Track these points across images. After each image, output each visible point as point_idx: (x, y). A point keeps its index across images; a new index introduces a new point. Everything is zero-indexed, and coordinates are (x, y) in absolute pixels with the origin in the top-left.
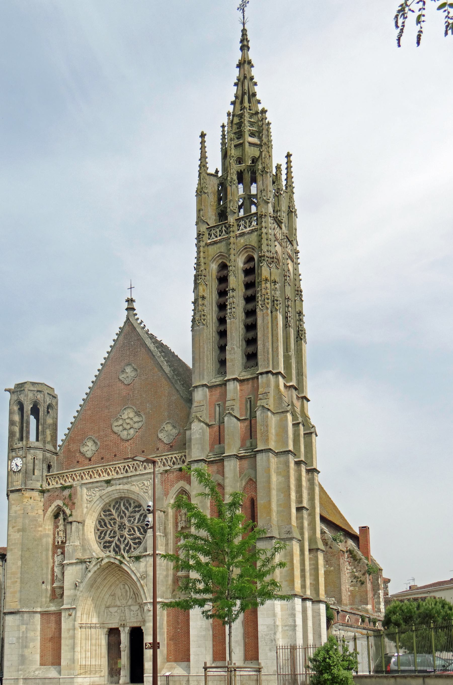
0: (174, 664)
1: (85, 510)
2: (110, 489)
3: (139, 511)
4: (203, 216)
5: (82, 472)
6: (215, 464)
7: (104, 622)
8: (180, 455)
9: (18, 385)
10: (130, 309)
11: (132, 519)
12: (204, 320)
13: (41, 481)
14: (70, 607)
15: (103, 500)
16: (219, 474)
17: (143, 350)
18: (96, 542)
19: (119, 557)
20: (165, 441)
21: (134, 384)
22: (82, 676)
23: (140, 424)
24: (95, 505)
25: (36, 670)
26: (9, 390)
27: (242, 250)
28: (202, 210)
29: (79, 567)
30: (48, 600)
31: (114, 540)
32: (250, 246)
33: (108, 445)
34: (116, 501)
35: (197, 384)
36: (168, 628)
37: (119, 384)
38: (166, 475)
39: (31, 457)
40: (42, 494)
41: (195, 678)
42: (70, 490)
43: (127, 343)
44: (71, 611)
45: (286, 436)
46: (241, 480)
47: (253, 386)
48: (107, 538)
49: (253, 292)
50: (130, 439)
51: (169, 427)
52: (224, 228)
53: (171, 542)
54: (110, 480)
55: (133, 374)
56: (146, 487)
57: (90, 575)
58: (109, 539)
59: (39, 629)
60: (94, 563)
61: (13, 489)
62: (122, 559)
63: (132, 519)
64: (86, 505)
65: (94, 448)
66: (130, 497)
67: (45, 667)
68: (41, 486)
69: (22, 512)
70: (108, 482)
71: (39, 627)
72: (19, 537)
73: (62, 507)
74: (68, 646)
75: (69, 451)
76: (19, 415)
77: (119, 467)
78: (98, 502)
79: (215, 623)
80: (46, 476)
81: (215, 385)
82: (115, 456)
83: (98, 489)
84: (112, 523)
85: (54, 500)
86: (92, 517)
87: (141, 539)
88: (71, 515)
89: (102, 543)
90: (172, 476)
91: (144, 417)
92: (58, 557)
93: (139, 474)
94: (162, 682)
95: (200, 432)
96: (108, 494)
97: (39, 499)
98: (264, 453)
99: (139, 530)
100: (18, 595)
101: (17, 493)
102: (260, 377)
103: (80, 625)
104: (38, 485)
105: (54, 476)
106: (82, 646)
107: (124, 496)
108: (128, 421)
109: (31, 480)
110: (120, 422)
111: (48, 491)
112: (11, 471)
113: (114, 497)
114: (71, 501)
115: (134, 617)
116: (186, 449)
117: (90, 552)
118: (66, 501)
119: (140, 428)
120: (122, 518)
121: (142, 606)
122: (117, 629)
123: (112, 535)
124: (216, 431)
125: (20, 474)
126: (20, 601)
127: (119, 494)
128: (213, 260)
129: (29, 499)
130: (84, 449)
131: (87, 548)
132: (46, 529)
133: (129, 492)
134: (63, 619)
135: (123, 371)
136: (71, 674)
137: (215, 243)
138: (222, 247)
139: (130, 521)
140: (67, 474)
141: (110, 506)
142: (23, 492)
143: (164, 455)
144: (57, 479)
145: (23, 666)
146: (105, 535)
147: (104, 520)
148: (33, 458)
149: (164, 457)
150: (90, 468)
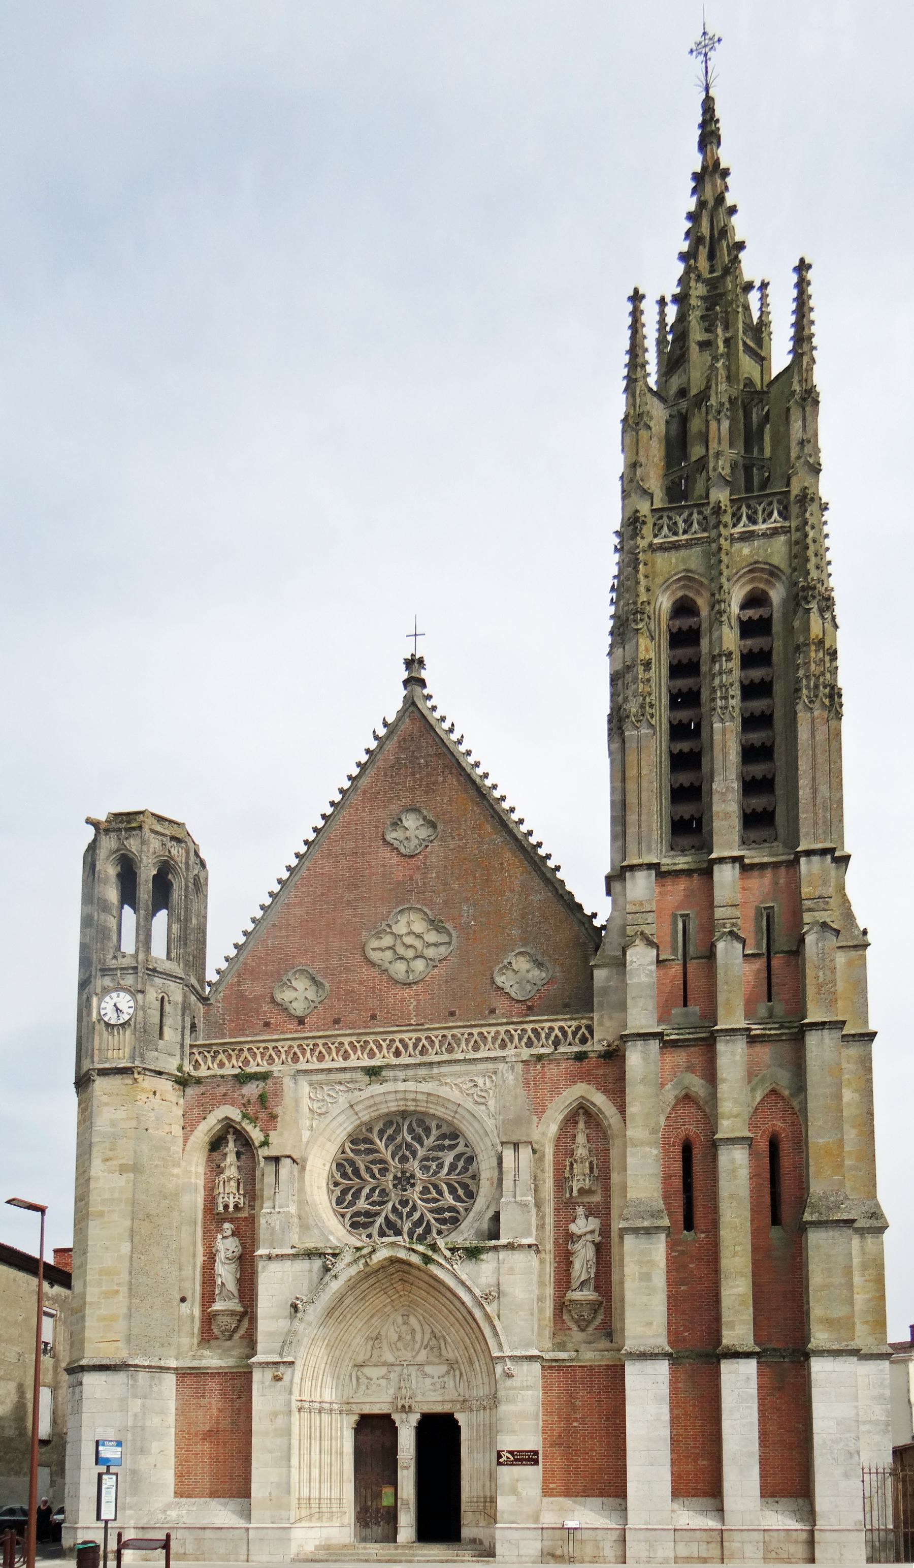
0: (567, 1502)
1: (306, 1135)
2: (377, 1089)
3: (451, 1148)
4: (642, 480)
5: (295, 1044)
6: (681, 1049)
7: (352, 1400)
8: (575, 1024)
9: (116, 815)
10: (414, 682)
11: (434, 1165)
12: (652, 717)
13: (178, 1057)
14: (278, 1359)
15: (356, 1114)
16: (693, 1072)
17: (452, 781)
18: (331, 1212)
19: (421, 1248)
20: (513, 995)
21: (426, 857)
22: (303, 1524)
23: (443, 950)
24: (334, 1123)
25: (168, 1506)
26: (95, 824)
27: (745, 573)
28: (641, 466)
29: (303, 1265)
30: (196, 1341)
31: (382, 1210)
32: (767, 567)
33: (353, 991)
34: (387, 1119)
35: (636, 861)
36: (545, 1418)
37: (386, 852)
38: (539, 1067)
39: (155, 995)
40: (182, 1088)
41: (641, 1536)
42: (262, 1084)
43: (406, 759)
44: (282, 1368)
45: (862, 1001)
46: (753, 1090)
47: (776, 883)
48: (362, 1204)
49: (768, 675)
50: (415, 983)
51: (522, 964)
52: (695, 516)
53: (550, 1220)
54: (380, 1067)
55: (424, 833)
56: (482, 1090)
57: (335, 1286)
58: (369, 1207)
59: (173, 1411)
60: (348, 1257)
61: (107, 1066)
62: (430, 1253)
63: (434, 1165)
64: (308, 1123)
65: (311, 995)
66: (432, 1111)
67: (193, 1500)
68: (180, 1069)
69: (134, 1124)
70: (373, 1072)
71: (172, 1405)
72: (123, 1184)
73: (239, 1123)
74: (270, 1452)
75: (241, 996)
76: (117, 889)
77: (401, 1041)
78: (342, 1118)
79: (676, 1412)
80: (191, 1046)
81: (675, 871)
82: (374, 1017)
83: (342, 1088)
84: (376, 1171)
85: (214, 1107)
86: (324, 1152)
87: (458, 1212)
88: (265, 1143)
89: (348, 1216)
90: (553, 1071)
91: (454, 933)
92: (225, 1241)
93: (465, 1060)
94: (546, 1543)
95: (651, 971)
96: (372, 1102)
97: (174, 1100)
98: (826, 1032)
99: (452, 1190)
100: (121, 1326)
101: (119, 1077)
102: (803, 860)
103: (299, 1404)
104: (171, 1065)
105: (214, 1048)
106: (302, 1452)
107: (412, 1108)
108: (409, 940)
109: (156, 1050)
110: (387, 941)
111: (199, 1081)
112: (99, 1021)
113: (386, 1110)
114: (265, 1109)
115: (435, 1390)
116: (592, 1011)
117: (323, 1234)
118: (251, 1110)
119: (443, 959)
120: (404, 1159)
121: (455, 1366)
122: (388, 1416)
123: (375, 1197)
124: (675, 976)
125: (128, 1033)
126: (128, 1339)
127: (401, 1103)
128: (667, 585)
129: (151, 1096)
130: (284, 996)
131: (311, 1222)
132: (190, 1172)
133: (431, 1099)
134: (255, 1387)
135: (397, 824)
136: (281, 1520)
137: (675, 546)
138: (693, 559)
139: (427, 1168)
140: (251, 1046)
141: (370, 1130)
142: (136, 1076)
143: (531, 1022)
144: (221, 1056)
145: (135, 1499)
146: (356, 1196)
147: (352, 1163)
148: (160, 997)
149: (532, 1026)
150: (320, 1037)
